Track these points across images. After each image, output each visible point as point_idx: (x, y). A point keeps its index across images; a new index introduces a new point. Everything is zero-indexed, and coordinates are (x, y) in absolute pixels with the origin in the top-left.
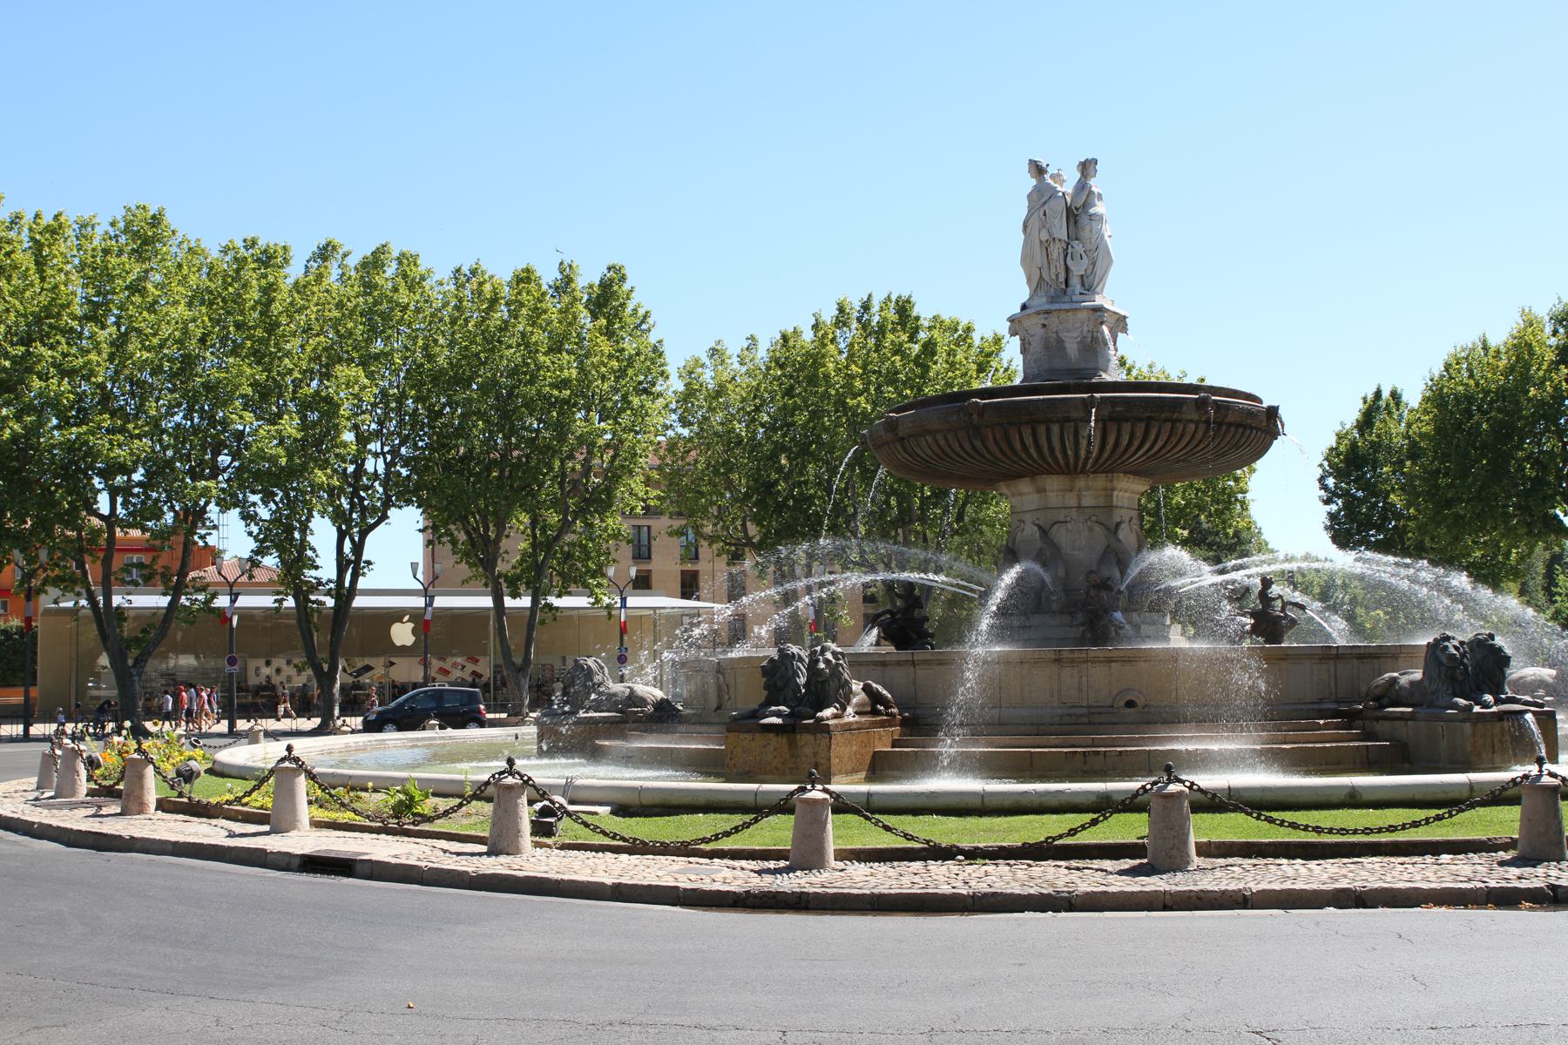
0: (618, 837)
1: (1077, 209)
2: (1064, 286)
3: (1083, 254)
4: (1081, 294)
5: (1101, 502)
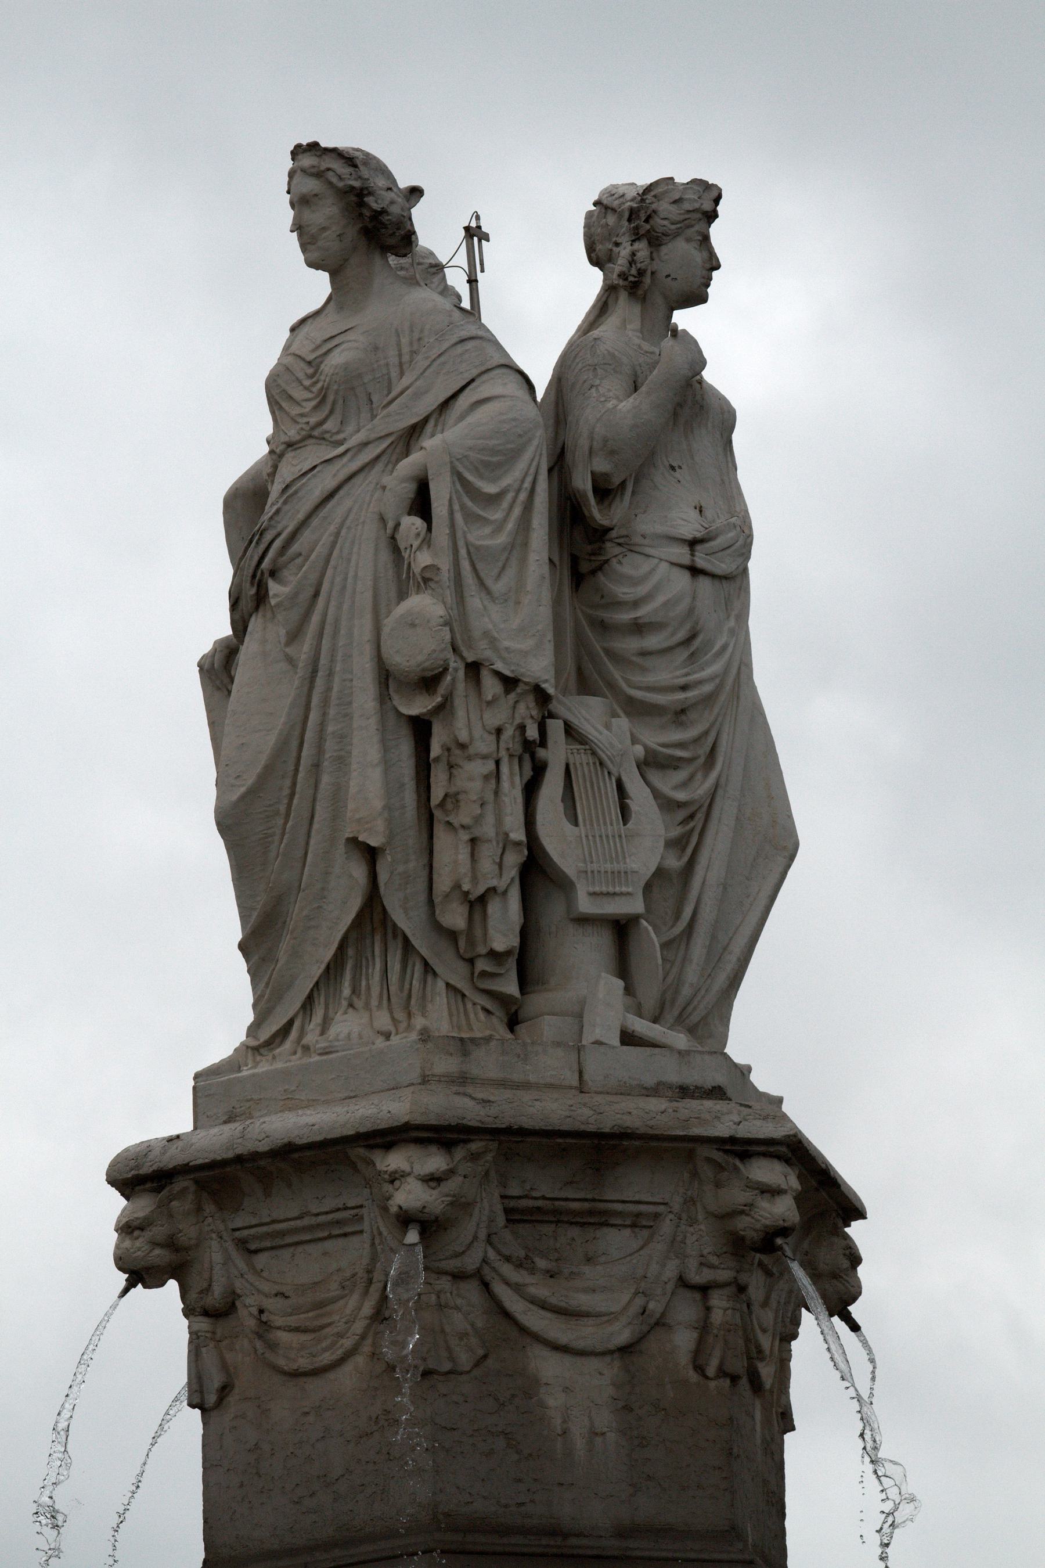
1: (604, 491)
2: (511, 987)
3: (635, 786)
4: (628, 1038)
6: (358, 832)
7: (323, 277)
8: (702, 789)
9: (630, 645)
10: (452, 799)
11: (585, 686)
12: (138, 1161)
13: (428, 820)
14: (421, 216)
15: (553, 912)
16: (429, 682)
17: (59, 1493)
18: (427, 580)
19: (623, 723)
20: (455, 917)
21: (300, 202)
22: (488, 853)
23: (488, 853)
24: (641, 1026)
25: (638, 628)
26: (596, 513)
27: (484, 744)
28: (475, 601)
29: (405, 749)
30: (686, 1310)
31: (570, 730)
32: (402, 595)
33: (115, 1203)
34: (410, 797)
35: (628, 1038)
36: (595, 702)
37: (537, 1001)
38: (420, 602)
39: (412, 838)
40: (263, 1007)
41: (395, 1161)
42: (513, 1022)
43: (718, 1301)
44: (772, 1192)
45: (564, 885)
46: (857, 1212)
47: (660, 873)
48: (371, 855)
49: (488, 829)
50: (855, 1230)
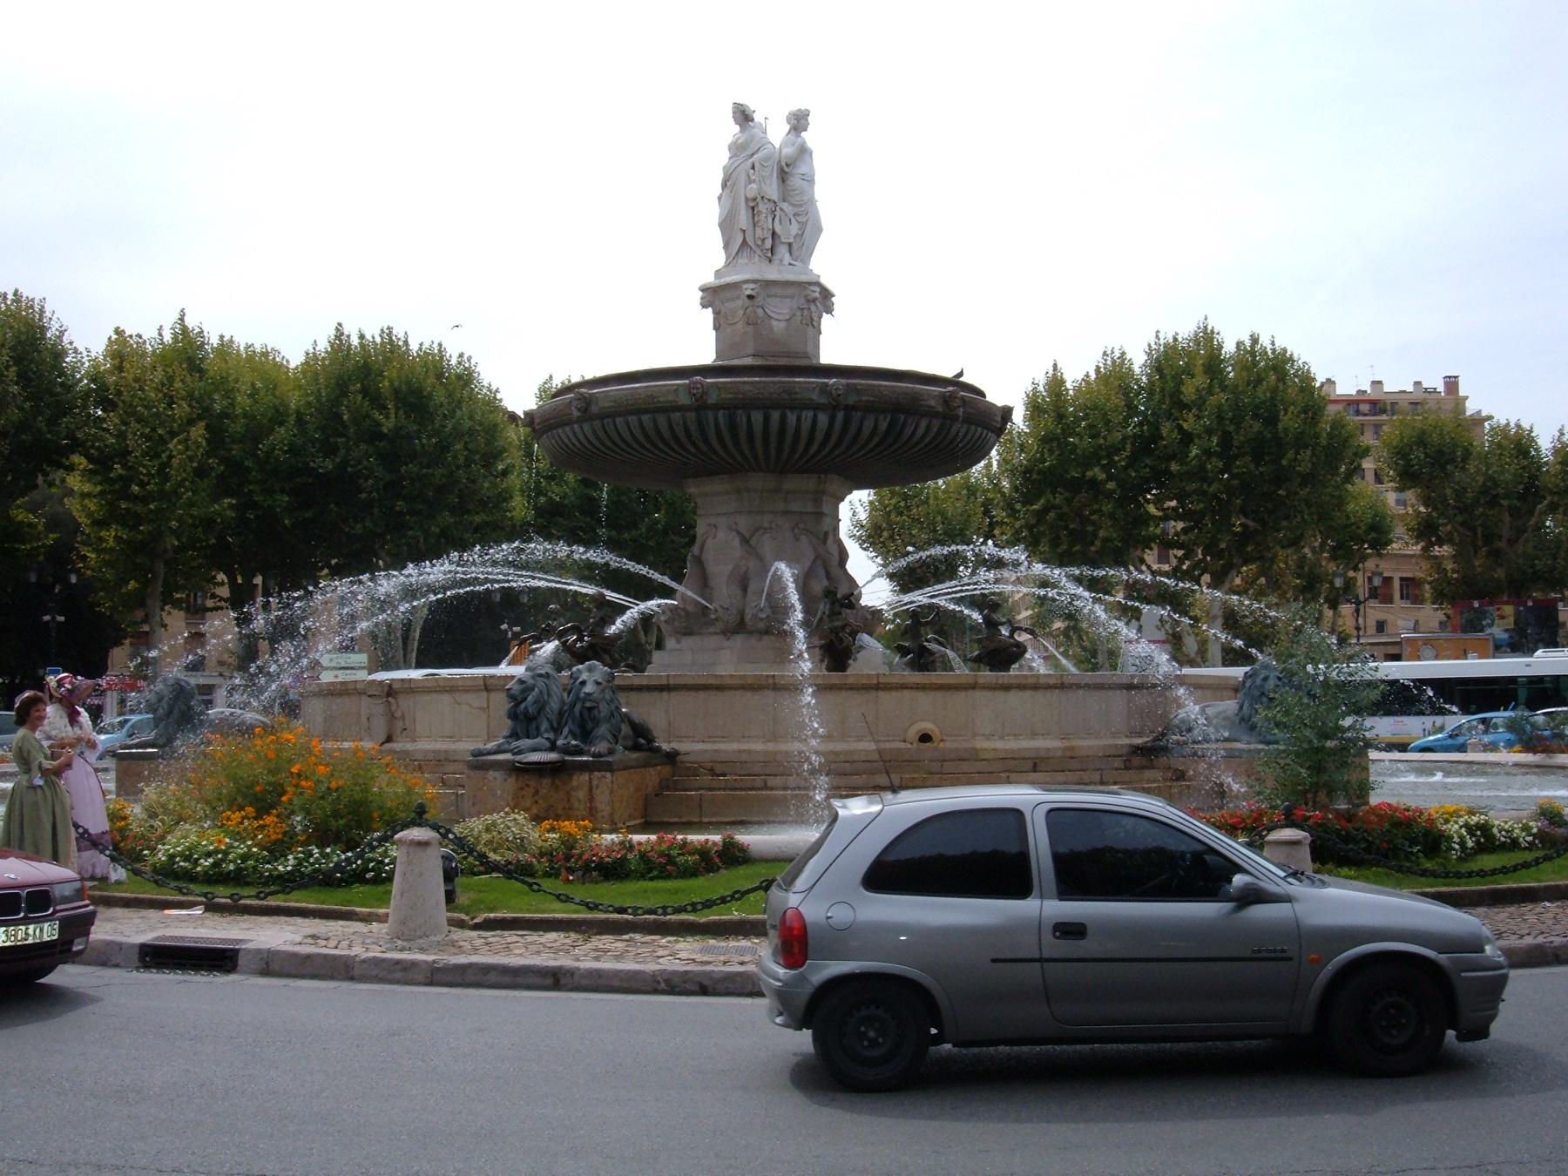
0: (669, 910)
1: (787, 165)
2: (769, 255)
3: (793, 219)
4: (790, 264)
5: (810, 508)
6: (203, 919)
7: (738, 127)
8: (804, 220)
9: (792, 193)
10: (759, 221)
11: (784, 201)
12: (294, 733)
13: (754, 225)
14: (755, 116)
15: (777, 242)
16: (755, 199)
17: (1520, 982)
18: (754, 181)
19: (790, 208)
20: (760, 243)
21: (734, 113)
22: (765, 232)
23: (765, 232)
24: (793, 262)
25: (794, 190)
26: (786, 169)
27: (765, 211)
28: (763, 185)
29: (750, 210)
30: (799, 313)
31: (781, 209)
32: (750, 183)
33: (700, 294)
34: (751, 221)
35: (790, 264)
36: (785, 204)
37: (775, 257)
38: (753, 185)
39: (751, 228)
40: (727, 259)
41: (745, 286)
42: (770, 261)
43: (805, 312)
44: (814, 292)
45: (779, 237)
46: (833, 296)
47: (797, 235)
48: (744, 231)
49: (765, 226)
50: (833, 299)
